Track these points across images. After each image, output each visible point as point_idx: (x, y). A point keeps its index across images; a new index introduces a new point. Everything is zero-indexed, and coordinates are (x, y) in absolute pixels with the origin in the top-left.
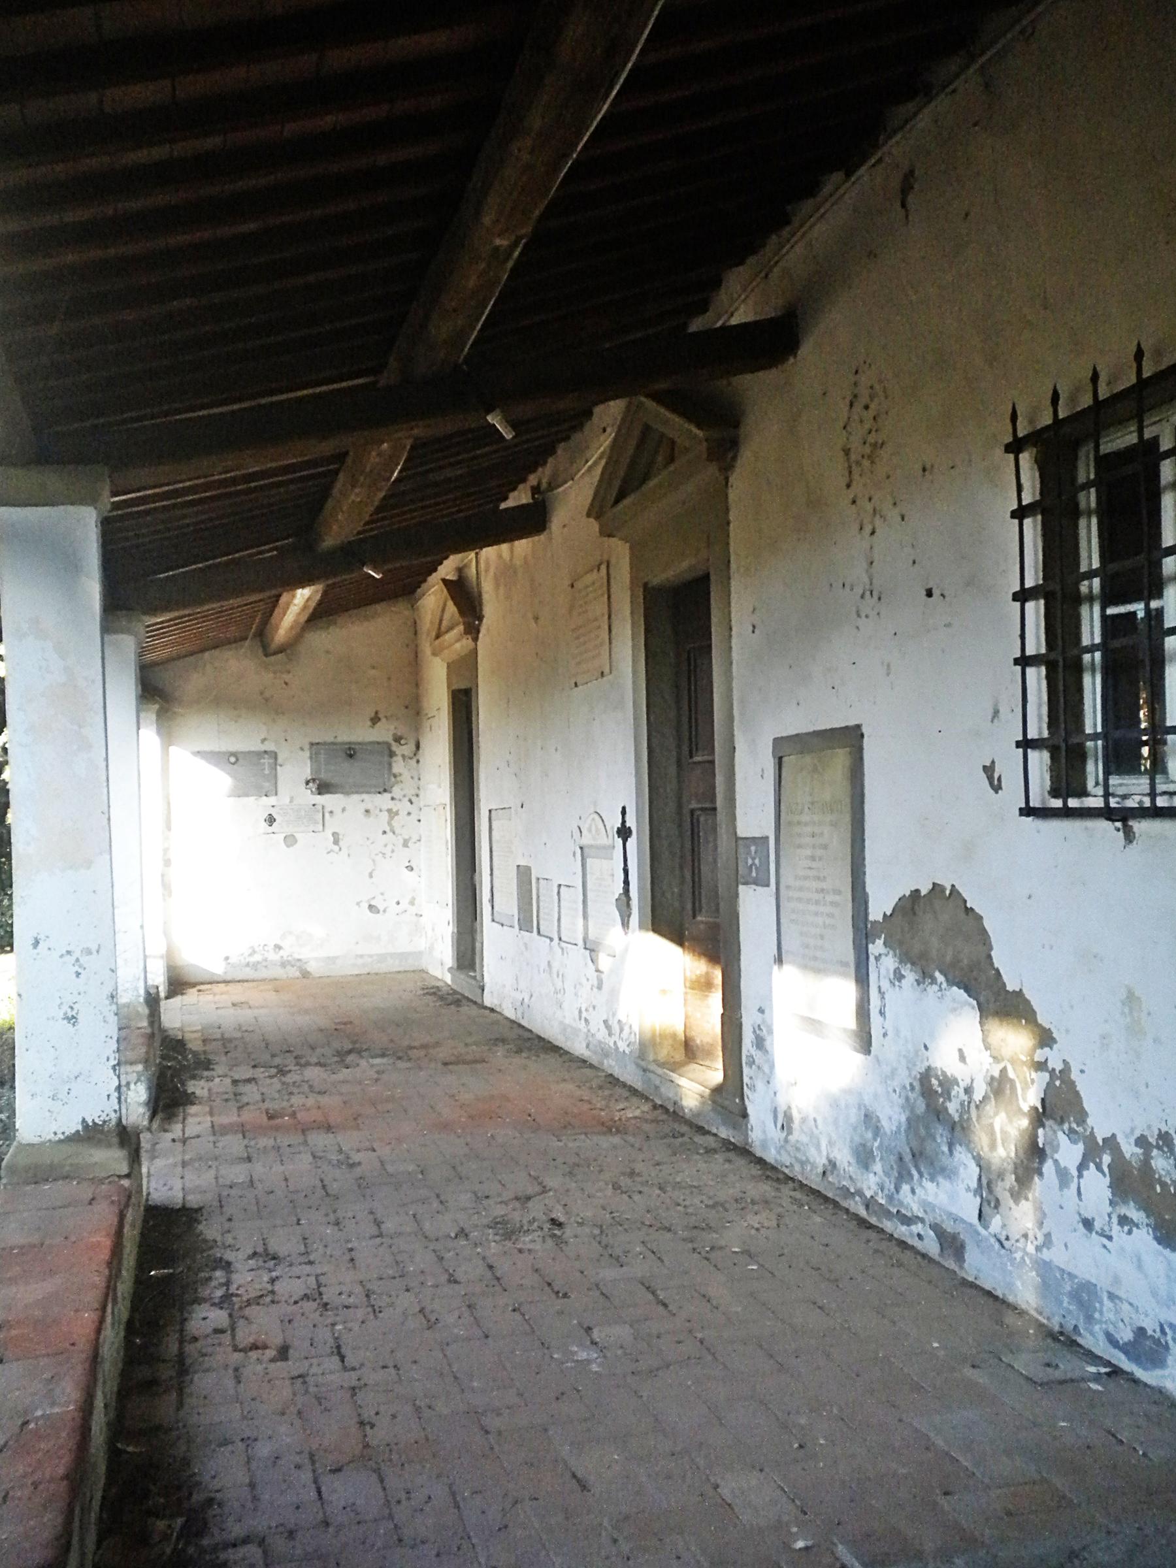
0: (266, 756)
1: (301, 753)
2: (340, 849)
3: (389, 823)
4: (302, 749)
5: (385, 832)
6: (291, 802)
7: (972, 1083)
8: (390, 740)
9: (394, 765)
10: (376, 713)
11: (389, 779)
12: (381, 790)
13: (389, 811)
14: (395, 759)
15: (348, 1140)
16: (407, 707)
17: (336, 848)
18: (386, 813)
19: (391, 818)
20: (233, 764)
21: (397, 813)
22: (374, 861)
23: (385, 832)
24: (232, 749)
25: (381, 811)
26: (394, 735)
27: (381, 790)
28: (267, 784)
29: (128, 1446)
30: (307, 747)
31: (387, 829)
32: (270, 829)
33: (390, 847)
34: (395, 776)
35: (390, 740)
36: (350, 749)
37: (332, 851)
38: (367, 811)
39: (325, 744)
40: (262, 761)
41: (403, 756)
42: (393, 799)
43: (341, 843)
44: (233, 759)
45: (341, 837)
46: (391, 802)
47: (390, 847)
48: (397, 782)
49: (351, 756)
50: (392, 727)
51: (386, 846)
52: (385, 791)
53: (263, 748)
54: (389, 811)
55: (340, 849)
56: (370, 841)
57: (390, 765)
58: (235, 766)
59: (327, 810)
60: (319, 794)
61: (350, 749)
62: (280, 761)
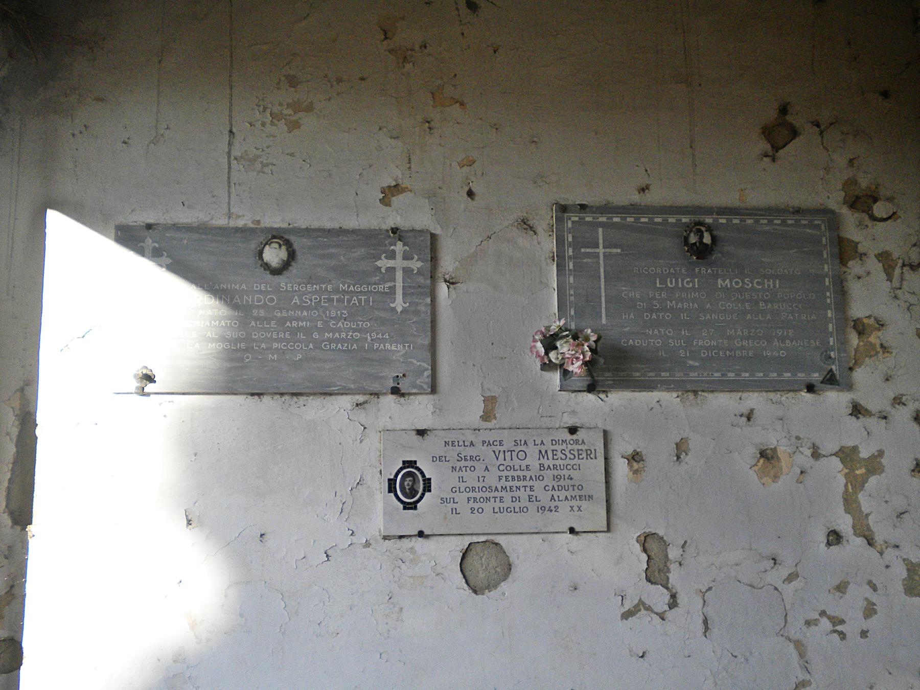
0: (399, 247)
1: (524, 240)
2: (673, 603)
3: (850, 503)
4: (526, 225)
5: (835, 537)
6: (487, 416)
7: (824, 456)
8: (834, 200)
9: (855, 289)
10: (784, 110)
11: (843, 343)
12: (816, 377)
13: (847, 455)
14: (855, 267)
15: (491, 566)
16: (885, 94)
17: (657, 596)
18: (836, 463)
19: (855, 484)
20: (276, 272)
21: (874, 465)
22: (800, 646)
23: (835, 537)
24: (274, 220)
25: (816, 454)
26: (850, 183)
27: (816, 377)
28: (397, 349)
29: (420, 365)
30: (544, 220)
31: (845, 524)
32: (410, 522)
33: (858, 594)
34: (861, 329)
35: (834, 200)
36: (698, 227)
37: (641, 606)
38: (767, 455)
39: (606, 209)
40: (384, 263)
41: (884, 257)
42: (857, 410)
43: (675, 576)
44: (274, 255)
45: (674, 553)
46: (853, 424)
47: (858, 594)
48: (870, 351)
49: (702, 252)
50: (841, 160)
51: (841, 588)
52: (831, 380)
53: (392, 218)
54: (847, 455)
55: (673, 603)
56: (784, 572)
57: (842, 293)
58: (281, 281)
59: (622, 447)
60: (844, 593)
61: (698, 227)
62: (448, 264)
